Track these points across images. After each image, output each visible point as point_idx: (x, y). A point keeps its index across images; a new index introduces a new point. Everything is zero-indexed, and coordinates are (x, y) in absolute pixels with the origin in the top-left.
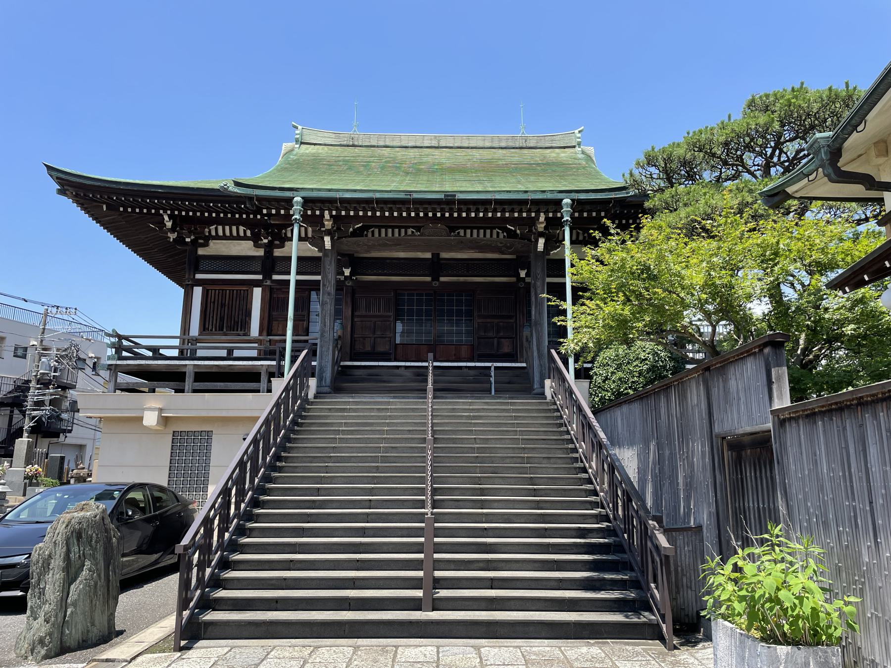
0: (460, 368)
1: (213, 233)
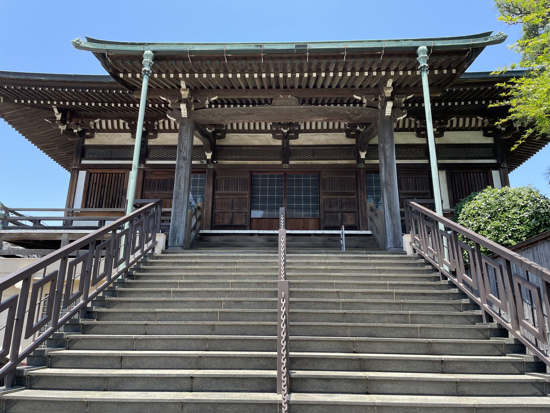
0: (309, 235)
1: (98, 127)
